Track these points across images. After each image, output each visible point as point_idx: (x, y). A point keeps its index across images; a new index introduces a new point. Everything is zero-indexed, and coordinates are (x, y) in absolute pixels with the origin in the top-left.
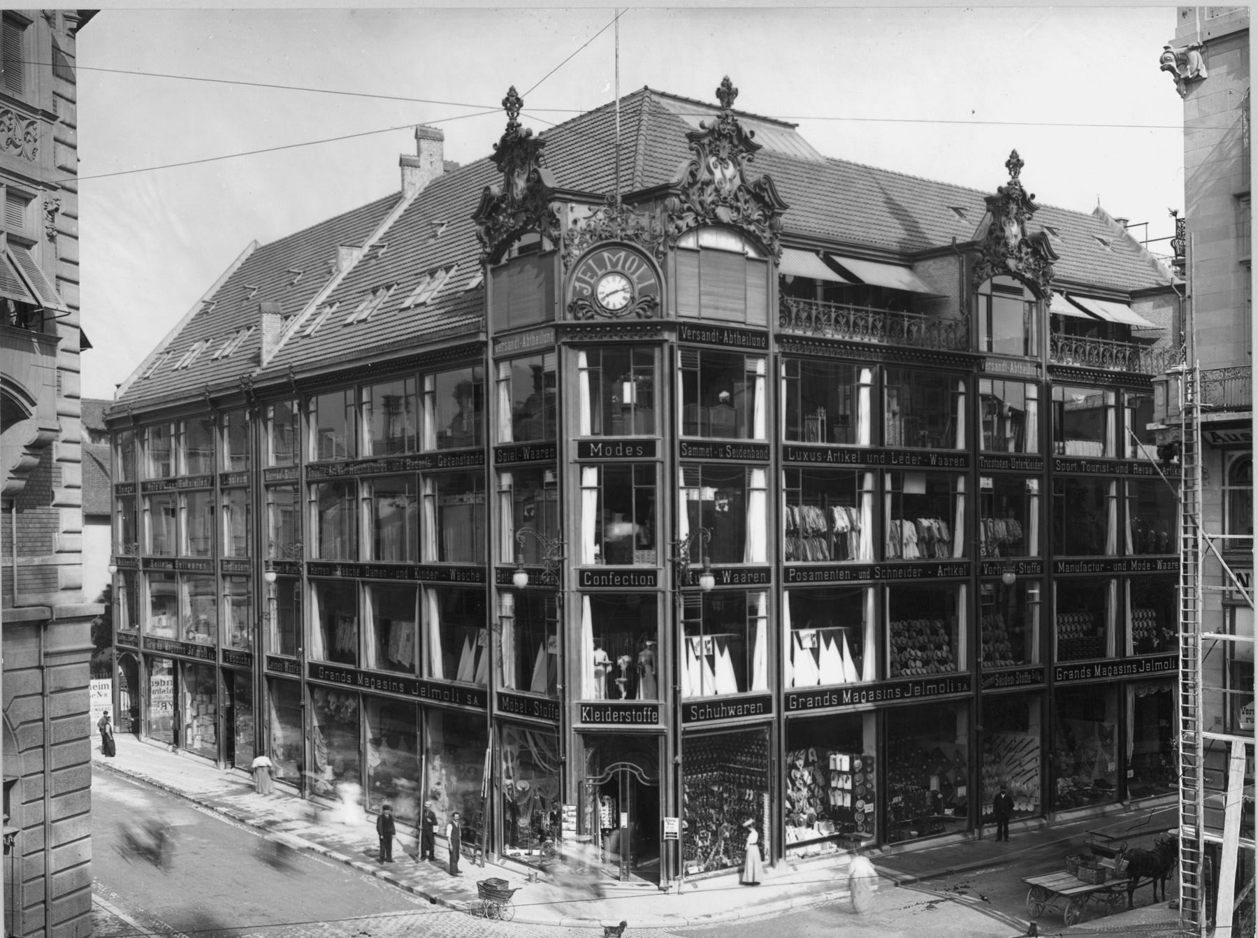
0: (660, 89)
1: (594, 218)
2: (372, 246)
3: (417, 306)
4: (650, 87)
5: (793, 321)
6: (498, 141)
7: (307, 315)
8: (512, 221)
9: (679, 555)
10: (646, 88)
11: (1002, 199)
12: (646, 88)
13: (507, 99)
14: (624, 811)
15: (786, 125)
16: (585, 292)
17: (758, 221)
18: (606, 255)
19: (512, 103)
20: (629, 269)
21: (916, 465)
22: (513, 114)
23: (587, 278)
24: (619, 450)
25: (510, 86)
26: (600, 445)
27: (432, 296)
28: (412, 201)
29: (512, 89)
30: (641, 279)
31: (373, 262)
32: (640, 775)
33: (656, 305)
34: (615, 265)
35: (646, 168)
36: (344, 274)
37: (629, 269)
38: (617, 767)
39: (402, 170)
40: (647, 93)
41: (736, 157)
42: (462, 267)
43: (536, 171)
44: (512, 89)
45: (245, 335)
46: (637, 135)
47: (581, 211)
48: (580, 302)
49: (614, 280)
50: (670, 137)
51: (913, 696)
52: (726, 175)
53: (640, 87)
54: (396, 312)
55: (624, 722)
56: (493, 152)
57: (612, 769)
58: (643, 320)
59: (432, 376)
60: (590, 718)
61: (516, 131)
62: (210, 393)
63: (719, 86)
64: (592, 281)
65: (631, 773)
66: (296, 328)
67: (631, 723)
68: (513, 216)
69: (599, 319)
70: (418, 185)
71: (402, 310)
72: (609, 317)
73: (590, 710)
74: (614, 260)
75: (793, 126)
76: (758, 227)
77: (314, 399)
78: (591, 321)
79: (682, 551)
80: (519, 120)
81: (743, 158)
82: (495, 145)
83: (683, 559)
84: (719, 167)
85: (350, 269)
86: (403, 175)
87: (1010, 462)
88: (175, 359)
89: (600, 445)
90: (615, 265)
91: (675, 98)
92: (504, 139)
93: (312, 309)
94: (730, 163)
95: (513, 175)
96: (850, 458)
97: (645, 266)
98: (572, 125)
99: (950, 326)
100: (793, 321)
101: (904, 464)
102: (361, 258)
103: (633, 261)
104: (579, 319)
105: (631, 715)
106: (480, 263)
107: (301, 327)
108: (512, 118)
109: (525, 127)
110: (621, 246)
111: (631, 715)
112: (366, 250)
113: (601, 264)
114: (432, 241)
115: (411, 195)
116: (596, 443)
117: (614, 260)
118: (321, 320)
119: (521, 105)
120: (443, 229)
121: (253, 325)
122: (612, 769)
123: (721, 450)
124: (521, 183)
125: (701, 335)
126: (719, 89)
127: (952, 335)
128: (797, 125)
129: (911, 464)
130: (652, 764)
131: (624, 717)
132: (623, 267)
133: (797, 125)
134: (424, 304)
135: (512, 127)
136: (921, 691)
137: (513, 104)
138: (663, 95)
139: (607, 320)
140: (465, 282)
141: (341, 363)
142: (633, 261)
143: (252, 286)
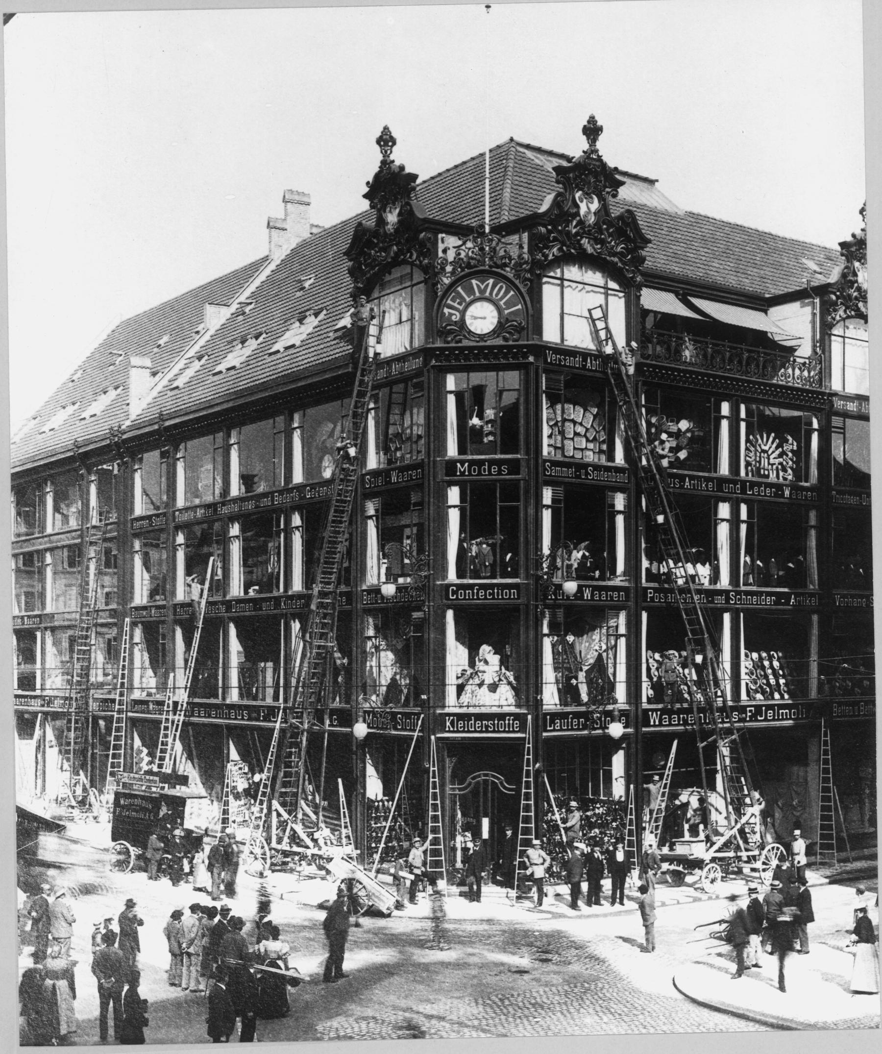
0: (526, 141)
1: (463, 247)
2: (240, 303)
3: (287, 348)
4: (515, 138)
5: (618, 900)
6: (371, 180)
7: (175, 370)
8: (383, 254)
9: (542, 569)
10: (512, 140)
11: (855, 244)
12: (512, 140)
13: (381, 137)
14: (486, 816)
15: (645, 180)
16: (453, 318)
17: (621, 253)
18: (474, 282)
19: (386, 140)
20: (497, 295)
21: (770, 496)
22: (386, 152)
23: (456, 305)
24: (485, 469)
25: (384, 125)
26: (466, 465)
27: (302, 339)
28: (278, 262)
29: (386, 128)
30: (509, 304)
31: (241, 318)
32: (501, 783)
33: (523, 328)
34: (483, 292)
35: (513, 208)
36: (212, 332)
37: (497, 295)
38: (479, 776)
39: (270, 232)
40: (513, 144)
41: (601, 192)
42: (331, 311)
43: (408, 204)
44: (386, 128)
45: (112, 394)
46: (504, 180)
47: (452, 241)
48: (449, 328)
49: (482, 307)
50: (535, 183)
51: (766, 720)
52: (588, 207)
53: (504, 139)
54: (266, 357)
55: (487, 731)
56: (367, 189)
57: (473, 778)
58: (511, 343)
59: (301, 412)
60: (453, 727)
61: (390, 168)
62: (79, 448)
63: (586, 123)
64: (461, 308)
65: (493, 782)
66: (165, 382)
67: (494, 731)
68: (385, 249)
69: (465, 343)
70: (285, 247)
71: (270, 354)
72: (478, 342)
73: (453, 720)
74: (482, 287)
75: (652, 182)
76: (621, 260)
77: (182, 446)
78: (460, 345)
79: (545, 565)
80: (392, 157)
81: (608, 193)
82: (368, 183)
83: (546, 573)
84: (585, 201)
85: (218, 327)
86: (270, 237)
87: (861, 499)
88: (43, 424)
89: (466, 465)
90: (483, 292)
91: (539, 150)
92: (377, 176)
93: (181, 365)
94: (594, 196)
95: (385, 212)
96: (707, 486)
97: (512, 293)
98: (438, 179)
99: (804, 364)
100: (618, 900)
101: (759, 495)
102: (229, 316)
103: (501, 288)
104: (448, 343)
105: (494, 725)
106: (351, 296)
107: (170, 381)
108: (386, 155)
109: (397, 163)
110: (489, 273)
111: (494, 725)
112: (234, 307)
113: (470, 290)
114: (299, 294)
115: (278, 256)
116: (462, 463)
117: (482, 287)
118: (190, 373)
119: (394, 143)
120: (312, 281)
121: (121, 385)
122: (473, 778)
123: (583, 471)
124: (392, 218)
125: (565, 360)
126: (585, 126)
127: (806, 373)
128: (657, 181)
129: (765, 495)
130: (514, 775)
131: (487, 727)
132: (491, 293)
133: (657, 181)
134: (293, 346)
135: (386, 163)
136: (774, 715)
137: (386, 144)
138: (528, 147)
139: (475, 344)
140: (334, 323)
141: (212, 406)
142: (501, 288)
143: (120, 352)
